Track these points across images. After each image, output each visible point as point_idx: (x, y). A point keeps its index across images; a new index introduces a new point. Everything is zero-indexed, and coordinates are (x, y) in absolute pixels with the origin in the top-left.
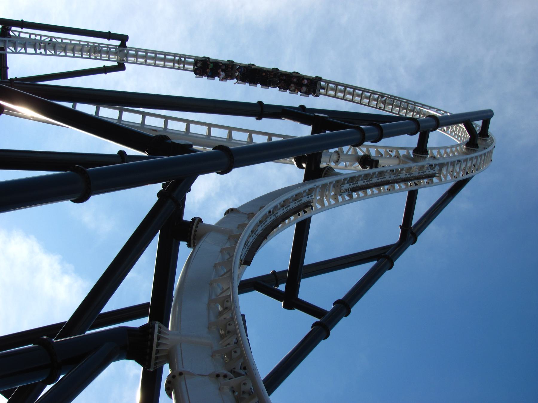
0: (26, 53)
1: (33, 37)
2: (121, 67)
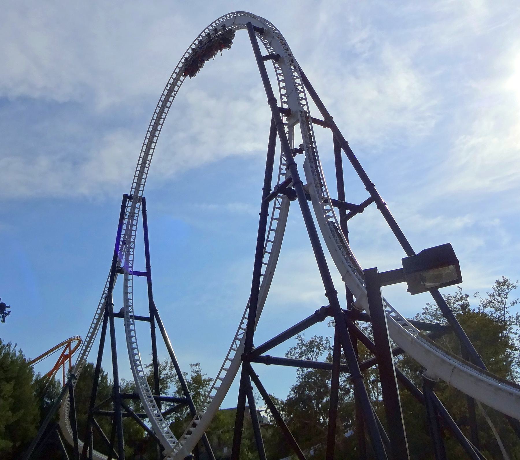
2: (143, 201)
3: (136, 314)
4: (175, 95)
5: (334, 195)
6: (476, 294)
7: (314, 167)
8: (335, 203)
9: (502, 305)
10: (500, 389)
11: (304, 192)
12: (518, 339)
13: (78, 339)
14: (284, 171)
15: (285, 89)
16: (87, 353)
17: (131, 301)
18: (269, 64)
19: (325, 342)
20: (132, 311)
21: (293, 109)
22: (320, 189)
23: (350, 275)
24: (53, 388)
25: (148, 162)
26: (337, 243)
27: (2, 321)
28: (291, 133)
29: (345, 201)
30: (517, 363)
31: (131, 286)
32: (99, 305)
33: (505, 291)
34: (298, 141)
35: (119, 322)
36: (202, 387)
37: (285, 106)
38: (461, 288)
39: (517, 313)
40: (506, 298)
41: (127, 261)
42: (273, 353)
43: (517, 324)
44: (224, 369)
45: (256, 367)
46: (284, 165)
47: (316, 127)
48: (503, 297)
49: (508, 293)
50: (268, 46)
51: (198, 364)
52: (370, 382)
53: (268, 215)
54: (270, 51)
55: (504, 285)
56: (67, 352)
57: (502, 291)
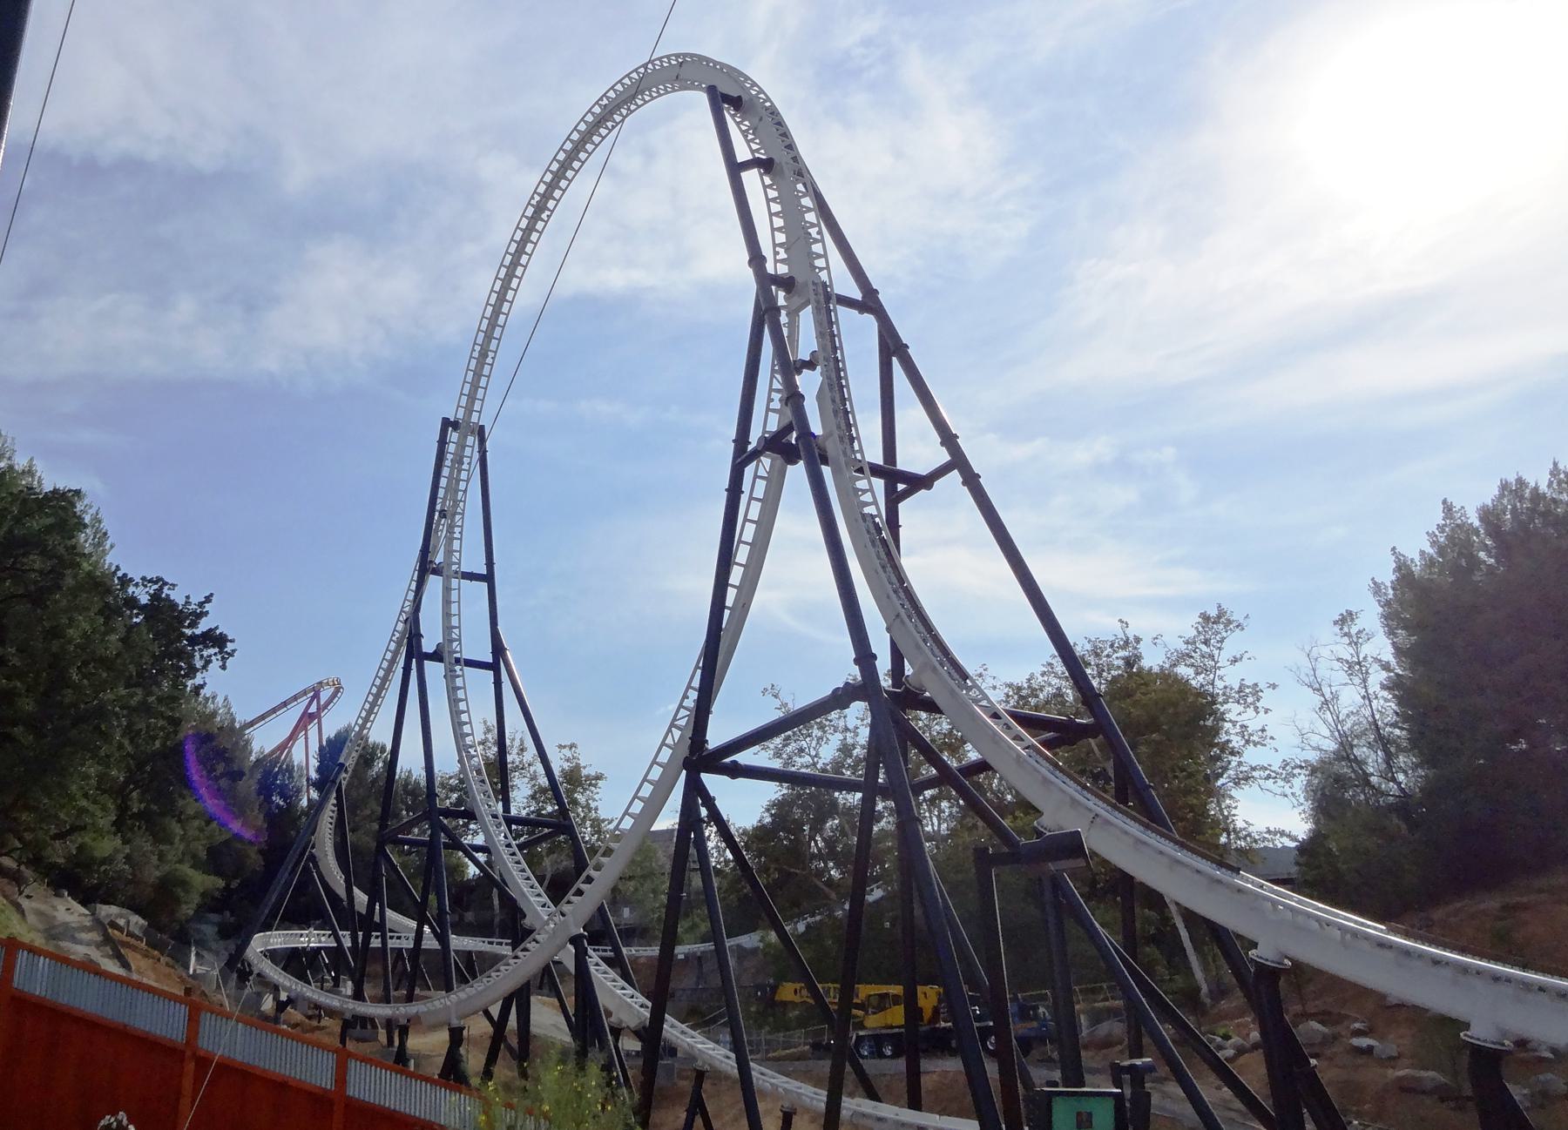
2: (481, 433)
3: (467, 655)
4: (549, 216)
5: (875, 455)
6: (1157, 638)
7: (838, 400)
8: (876, 471)
9: (1210, 662)
10: (1178, 862)
11: (816, 451)
12: (1240, 733)
13: (334, 685)
14: (776, 405)
15: (780, 217)
16: (368, 725)
17: (456, 631)
18: (751, 178)
19: (837, 716)
21: (799, 279)
22: (848, 447)
23: (903, 622)
24: (288, 778)
25: (491, 354)
26: (879, 558)
27: (220, 667)
28: (793, 325)
29: (895, 466)
30: (1234, 779)
32: (393, 635)
33: (1220, 633)
34: (807, 344)
35: (434, 670)
36: (582, 790)
37: (783, 269)
38: (1127, 623)
39: (1243, 680)
40: (1220, 649)
41: (449, 552)
42: (745, 758)
43: (1238, 702)
44: (649, 782)
45: (708, 779)
46: (778, 391)
47: (844, 314)
48: (1214, 646)
49: (1225, 638)
50: (750, 137)
51: (572, 746)
52: (925, 800)
53: (743, 492)
54: (754, 147)
55: (1219, 623)
56: (313, 709)
57: (1213, 634)
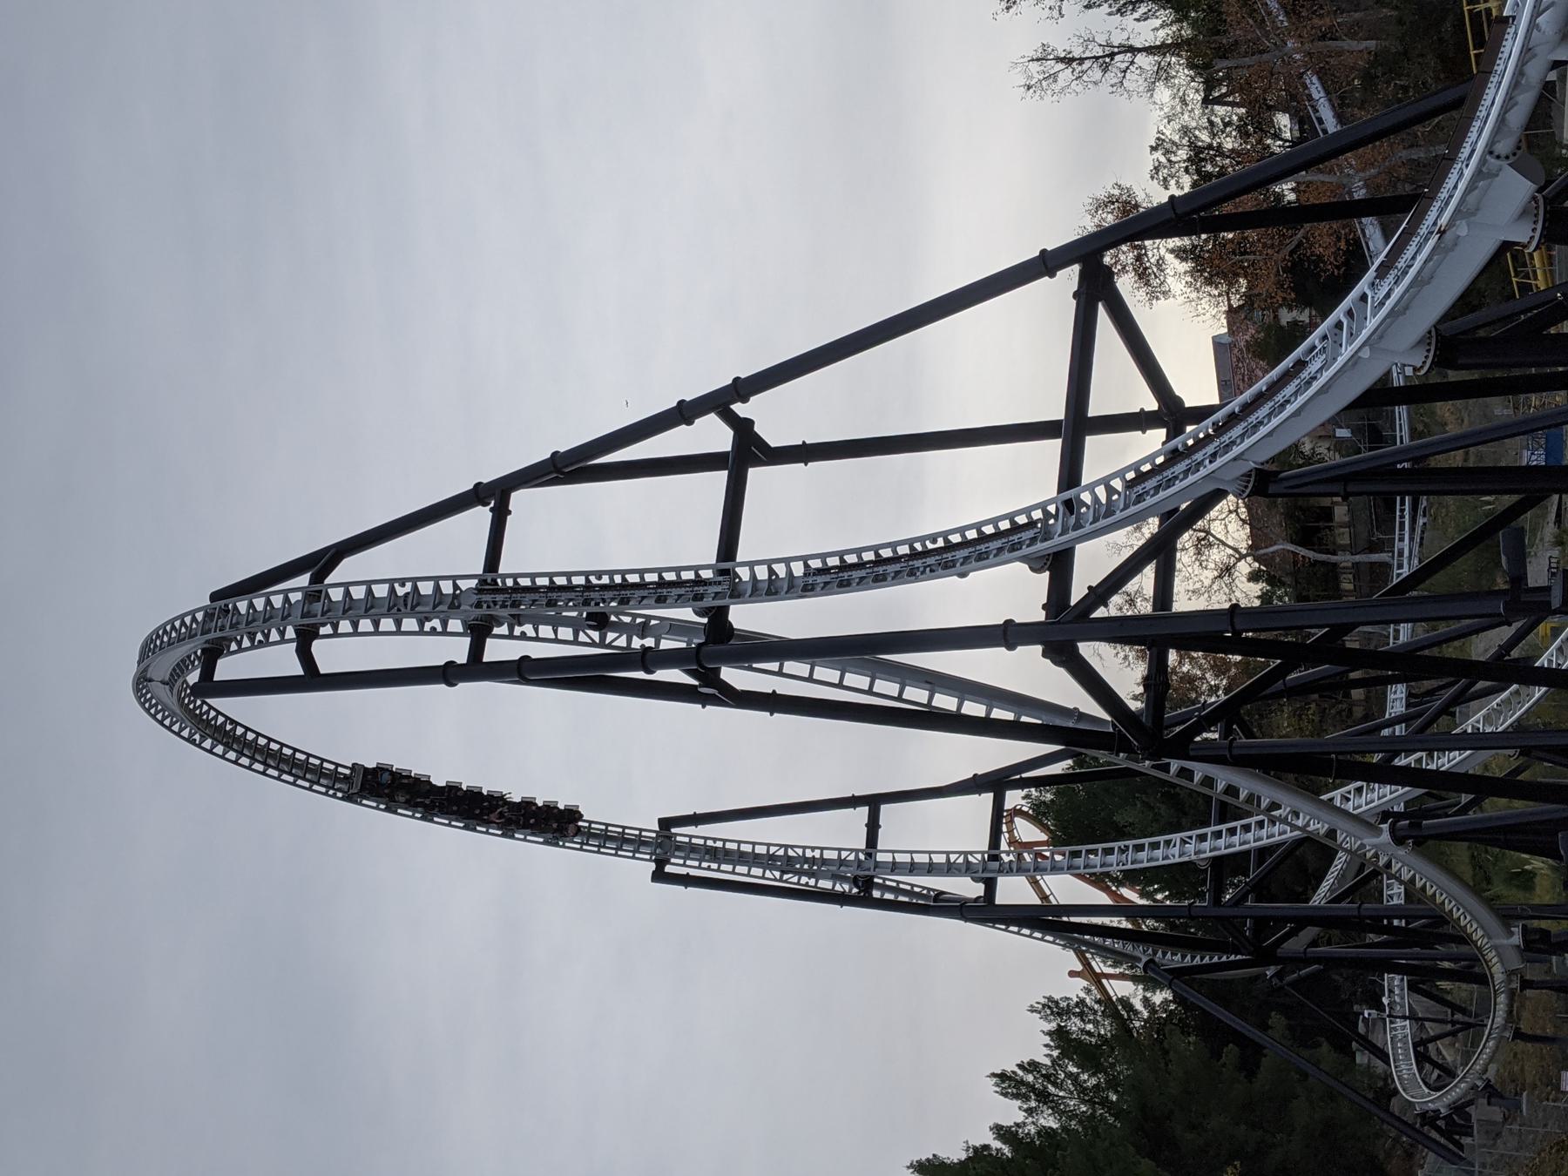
0: (948, 853)
1: (714, 866)
2: (666, 823)
20: (801, 850)
31: (928, 855)
